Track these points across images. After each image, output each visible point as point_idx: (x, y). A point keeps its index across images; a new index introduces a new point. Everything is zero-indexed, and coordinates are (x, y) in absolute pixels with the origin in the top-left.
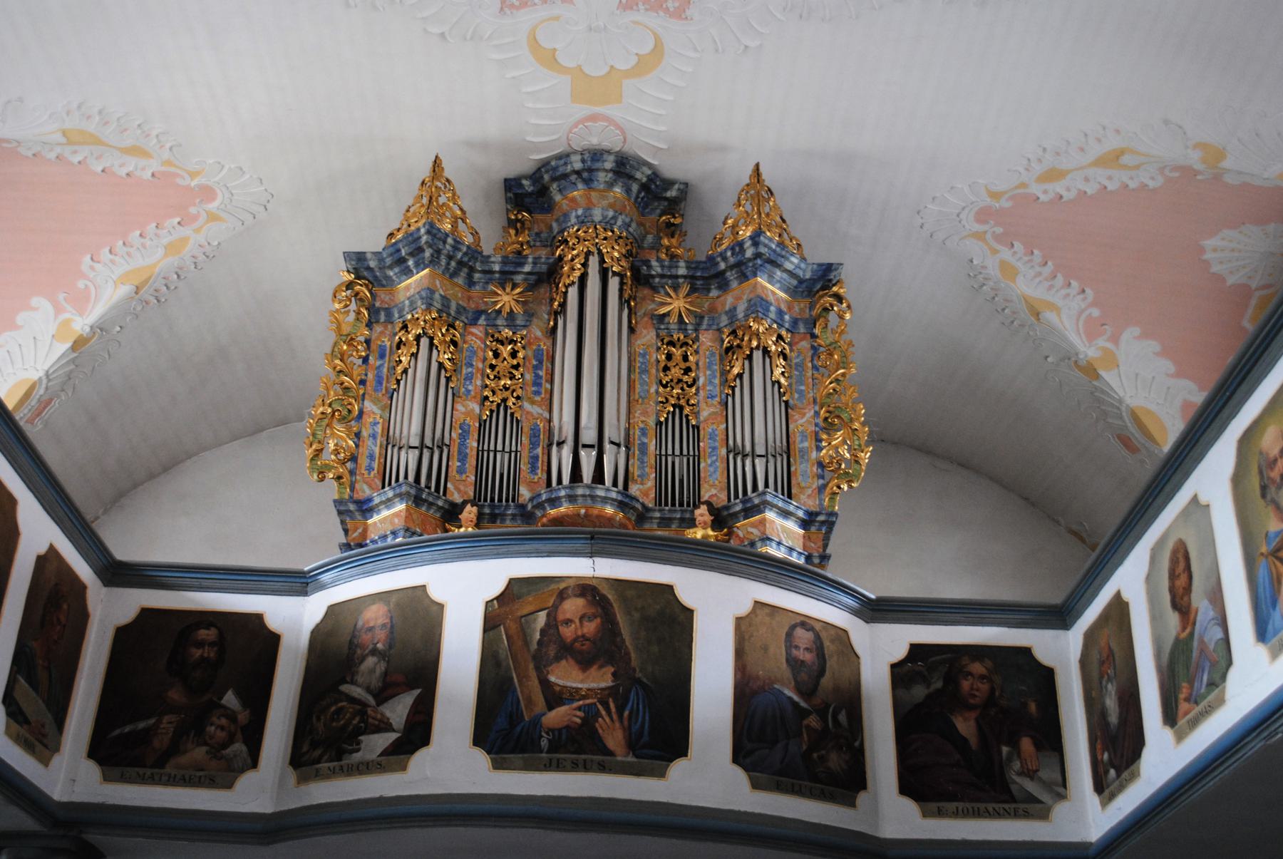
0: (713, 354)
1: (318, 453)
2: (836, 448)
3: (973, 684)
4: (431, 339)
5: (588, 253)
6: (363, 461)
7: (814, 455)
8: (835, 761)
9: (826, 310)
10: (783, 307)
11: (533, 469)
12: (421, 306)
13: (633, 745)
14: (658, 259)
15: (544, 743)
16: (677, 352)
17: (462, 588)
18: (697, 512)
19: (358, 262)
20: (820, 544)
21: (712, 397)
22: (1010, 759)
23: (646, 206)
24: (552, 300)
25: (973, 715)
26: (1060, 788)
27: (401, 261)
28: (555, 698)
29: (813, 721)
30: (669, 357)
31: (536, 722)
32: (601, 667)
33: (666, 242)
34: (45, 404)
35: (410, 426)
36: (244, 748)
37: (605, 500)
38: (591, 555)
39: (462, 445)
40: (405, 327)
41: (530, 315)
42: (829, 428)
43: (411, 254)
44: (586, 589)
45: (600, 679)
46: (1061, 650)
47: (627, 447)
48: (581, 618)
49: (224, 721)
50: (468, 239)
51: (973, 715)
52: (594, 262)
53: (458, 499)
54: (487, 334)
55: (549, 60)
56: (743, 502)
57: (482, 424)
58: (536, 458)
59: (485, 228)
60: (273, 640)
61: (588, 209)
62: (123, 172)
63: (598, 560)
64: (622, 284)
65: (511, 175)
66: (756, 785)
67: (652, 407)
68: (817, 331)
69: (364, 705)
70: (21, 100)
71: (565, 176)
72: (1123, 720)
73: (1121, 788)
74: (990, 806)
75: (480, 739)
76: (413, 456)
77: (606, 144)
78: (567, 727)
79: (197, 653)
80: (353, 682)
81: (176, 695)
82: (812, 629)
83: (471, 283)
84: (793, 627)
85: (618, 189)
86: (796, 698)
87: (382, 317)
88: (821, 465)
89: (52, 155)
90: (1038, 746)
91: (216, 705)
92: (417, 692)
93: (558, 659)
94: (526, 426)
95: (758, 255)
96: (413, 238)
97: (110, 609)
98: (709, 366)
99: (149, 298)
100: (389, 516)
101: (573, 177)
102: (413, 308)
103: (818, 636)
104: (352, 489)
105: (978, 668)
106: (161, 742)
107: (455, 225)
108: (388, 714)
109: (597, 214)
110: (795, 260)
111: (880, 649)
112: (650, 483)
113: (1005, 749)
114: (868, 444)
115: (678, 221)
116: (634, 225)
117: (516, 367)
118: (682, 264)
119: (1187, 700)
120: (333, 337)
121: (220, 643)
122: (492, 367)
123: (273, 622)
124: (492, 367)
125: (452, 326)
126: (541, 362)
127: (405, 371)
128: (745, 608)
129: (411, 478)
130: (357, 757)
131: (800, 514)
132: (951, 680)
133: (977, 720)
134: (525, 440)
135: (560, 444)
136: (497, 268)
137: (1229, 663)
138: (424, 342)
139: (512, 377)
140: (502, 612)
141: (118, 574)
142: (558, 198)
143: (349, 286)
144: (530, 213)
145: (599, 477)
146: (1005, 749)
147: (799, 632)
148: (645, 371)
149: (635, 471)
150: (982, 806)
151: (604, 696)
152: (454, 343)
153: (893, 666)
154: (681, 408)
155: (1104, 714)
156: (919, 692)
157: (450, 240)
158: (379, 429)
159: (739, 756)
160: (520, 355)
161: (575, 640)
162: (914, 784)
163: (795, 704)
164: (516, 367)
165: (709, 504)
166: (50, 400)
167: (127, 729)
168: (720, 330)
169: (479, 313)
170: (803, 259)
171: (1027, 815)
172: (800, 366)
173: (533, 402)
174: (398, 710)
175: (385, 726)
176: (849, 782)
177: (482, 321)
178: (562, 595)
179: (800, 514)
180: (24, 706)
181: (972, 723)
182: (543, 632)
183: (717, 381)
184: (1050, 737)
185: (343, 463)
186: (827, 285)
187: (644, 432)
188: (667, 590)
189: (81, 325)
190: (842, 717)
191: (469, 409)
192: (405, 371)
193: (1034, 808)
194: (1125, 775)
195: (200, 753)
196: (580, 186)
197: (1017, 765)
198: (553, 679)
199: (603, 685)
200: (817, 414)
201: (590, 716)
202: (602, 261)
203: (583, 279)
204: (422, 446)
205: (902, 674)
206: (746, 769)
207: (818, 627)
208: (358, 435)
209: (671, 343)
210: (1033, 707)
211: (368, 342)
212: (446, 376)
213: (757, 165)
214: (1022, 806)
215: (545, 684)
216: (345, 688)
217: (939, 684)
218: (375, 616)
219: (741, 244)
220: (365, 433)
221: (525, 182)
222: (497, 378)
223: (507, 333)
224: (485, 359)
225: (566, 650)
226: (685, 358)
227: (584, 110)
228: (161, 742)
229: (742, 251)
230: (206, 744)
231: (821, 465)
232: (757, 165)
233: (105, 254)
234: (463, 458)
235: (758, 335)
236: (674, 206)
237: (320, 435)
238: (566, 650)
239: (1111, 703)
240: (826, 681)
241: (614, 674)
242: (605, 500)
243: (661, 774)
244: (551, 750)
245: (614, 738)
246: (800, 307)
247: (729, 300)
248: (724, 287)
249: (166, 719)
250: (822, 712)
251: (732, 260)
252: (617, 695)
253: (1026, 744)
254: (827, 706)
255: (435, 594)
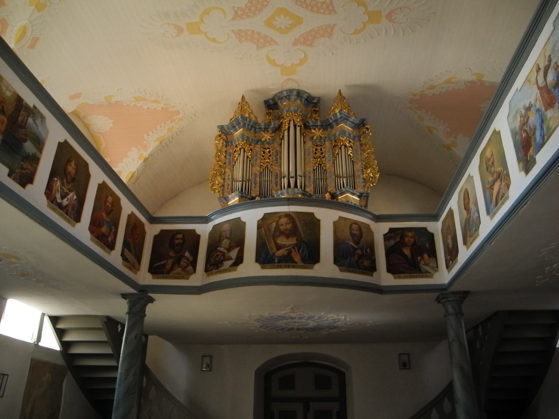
0: (330, 148)
1: (213, 185)
2: (368, 174)
3: (409, 239)
4: (244, 149)
5: (290, 121)
6: (226, 186)
7: (362, 176)
8: (366, 263)
9: (364, 133)
10: (350, 132)
11: (277, 185)
12: (241, 139)
13: (303, 260)
14: (312, 121)
15: (276, 261)
16: (319, 148)
17: (251, 217)
18: (326, 195)
19: (221, 128)
20: (365, 202)
21: (330, 161)
22: (421, 261)
23: (308, 105)
24: (280, 135)
25: (409, 248)
26: (436, 268)
27: (234, 127)
28: (279, 247)
29: (359, 251)
30: (316, 150)
31: (274, 255)
32: (293, 237)
33: (314, 116)
34: (138, 178)
35: (238, 174)
36: (191, 268)
37: (298, 193)
38: (289, 205)
39: (255, 180)
40: (236, 146)
41: (274, 140)
42: (366, 168)
43: (237, 125)
44: (288, 215)
45: (293, 241)
46: (435, 227)
47: (305, 177)
48: (286, 224)
49: (185, 260)
50: (254, 119)
51: (409, 248)
52: (292, 123)
53: (254, 195)
54: (261, 146)
55: (273, 63)
56: (340, 191)
57: (261, 173)
58: (277, 182)
59: (261, 117)
60: (199, 236)
61: (289, 107)
62: (153, 108)
63: (291, 207)
64: (301, 129)
65: (266, 99)
66: (341, 270)
67: (312, 165)
68: (361, 139)
69: (224, 253)
70: (121, 89)
71: (282, 98)
72: (453, 246)
73: (453, 267)
74: (415, 275)
75: (257, 260)
76: (240, 184)
77: (294, 88)
78: (283, 256)
79: (177, 242)
80: (221, 247)
81: (172, 254)
82: (357, 224)
83: (256, 132)
84: (351, 224)
85: (298, 101)
86: (353, 245)
87: (230, 144)
88: (364, 179)
89: (133, 105)
90: (429, 256)
91: (183, 256)
92: (239, 248)
93: (279, 236)
94: (274, 173)
95: (341, 117)
96: (237, 120)
97: (152, 231)
98: (329, 151)
99: (164, 145)
100: (234, 200)
101: (284, 98)
102: (238, 140)
103: (360, 227)
104: (223, 194)
105: (410, 234)
106: (168, 267)
107: (249, 115)
108: (231, 255)
109: (292, 109)
110: (353, 118)
111: (380, 230)
112: (312, 187)
113: (419, 258)
114: (378, 172)
115: (317, 109)
116: (304, 111)
117: (270, 156)
118: (319, 122)
119: (469, 236)
120: (215, 151)
121: (183, 238)
122: (263, 156)
123: (198, 232)
124: (263, 156)
125: (250, 145)
126: (277, 154)
127: (237, 159)
128: (336, 219)
129: (240, 190)
130: (222, 268)
131: (358, 194)
132: (402, 238)
133: (410, 250)
134: (274, 177)
135: (284, 177)
136: (263, 127)
137: (480, 223)
138: (242, 150)
139: (269, 159)
140: (262, 224)
141: (153, 220)
142: (280, 105)
143: (220, 136)
144: (272, 110)
145: (296, 186)
146: (419, 258)
147: (354, 225)
148: (309, 154)
149: (307, 183)
150: (412, 275)
151: (293, 246)
152: (251, 150)
153: (384, 235)
154: (321, 165)
155: (448, 245)
156: (392, 242)
157: (248, 120)
158: (230, 177)
159: (336, 262)
160: (271, 152)
161: (285, 230)
162: (391, 269)
163: (353, 247)
164: (270, 156)
165: (330, 193)
166: (139, 178)
167: (159, 264)
168: (331, 141)
169: (258, 141)
170: (356, 118)
171: (426, 277)
172: (356, 150)
173: (275, 166)
174: (234, 254)
175: (230, 259)
176: (372, 269)
177: (259, 143)
178: (280, 217)
179: (358, 194)
180: (128, 257)
181: (409, 251)
182: (275, 229)
183: (331, 156)
184: (433, 253)
185: (220, 187)
186: (364, 125)
187: (309, 172)
188: (312, 214)
189: (146, 154)
190: (368, 250)
191: (257, 169)
192: (237, 159)
193: (427, 274)
194: (454, 262)
195: (179, 270)
196: (287, 100)
197: (423, 262)
198: (278, 242)
199: (293, 243)
200: (362, 164)
201: (290, 252)
202: (294, 122)
203: (289, 128)
204: (243, 181)
205: (387, 237)
206: (338, 266)
207: (360, 224)
208: (224, 179)
209: (317, 146)
210: (427, 245)
211: (226, 151)
212: (249, 161)
213: (340, 91)
214: (425, 274)
215: (276, 244)
216: (219, 249)
217: (398, 240)
218: (226, 227)
219: (336, 114)
220: (226, 178)
221: (270, 101)
222: (265, 159)
223: (267, 146)
224: (261, 154)
225: (282, 233)
226: (321, 150)
227: (285, 78)
228: (168, 267)
229: (337, 116)
230: (180, 267)
231: (364, 179)
232: (340, 91)
233: (150, 133)
234: (255, 183)
235: (343, 141)
236: (316, 105)
237: (213, 179)
238: (282, 233)
239: (450, 242)
240: (363, 240)
241: (297, 240)
242: (298, 193)
243: (312, 268)
244: (279, 262)
245: (297, 258)
246: (356, 133)
247: (334, 131)
248: (332, 127)
249: (169, 261)
250: (362, 249)
251: (334, 119)
252: (298, 246)
253: (426, 256)
254: (363, 247)
255: (243, 219)
